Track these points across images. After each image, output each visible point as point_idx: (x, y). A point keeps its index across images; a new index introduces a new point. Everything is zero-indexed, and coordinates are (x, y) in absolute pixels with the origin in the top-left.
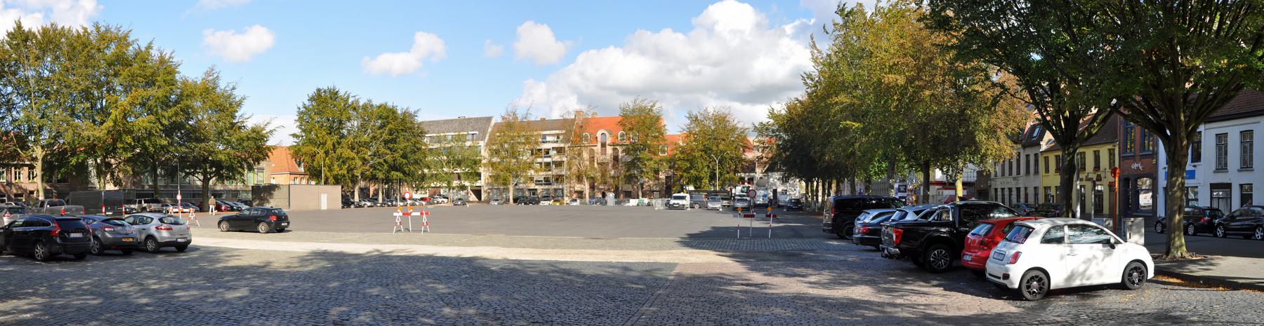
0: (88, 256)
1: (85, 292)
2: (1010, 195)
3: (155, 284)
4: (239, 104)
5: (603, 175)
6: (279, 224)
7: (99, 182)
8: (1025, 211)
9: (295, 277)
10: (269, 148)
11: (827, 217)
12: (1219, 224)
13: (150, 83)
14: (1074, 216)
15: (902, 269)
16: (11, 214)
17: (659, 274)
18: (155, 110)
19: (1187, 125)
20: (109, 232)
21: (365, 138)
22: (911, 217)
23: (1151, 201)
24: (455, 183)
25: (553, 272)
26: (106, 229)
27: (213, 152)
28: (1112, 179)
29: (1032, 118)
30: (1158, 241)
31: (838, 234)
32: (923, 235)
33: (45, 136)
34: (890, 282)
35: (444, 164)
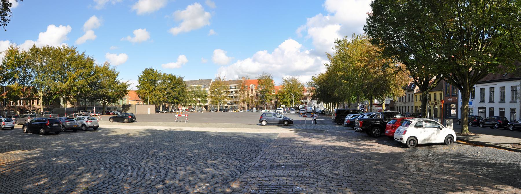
0: (60, 133)
1: (59, 146)
2: (403, 109)
3: (85, 142)
4: (117, 75)
5: (252, 101)
6: (132, 119)
7: (64, 105)
8: (408, 115)
9: (138, 139)
10: (128, 91)
11: (334, 117)
12: (481, 122)
13: (84, 67)
14: (427, 117)
15: (363, 136)
16: (31, 117)
17: (271, 138)
18: (85, 77)
19: (469, 85)
20: (68, 123)
21: (164, 87)
22: (366, 117)
23: (455, 113)
24: (198, 104)
25: (235, 136)
26: (67, 122)
27: (107, 93)
28: (441, 104)
29: (410, 81)
30: (458, 127)
31: (338, 123)
32: (370, 123)
33: (43, 89)
34: (358, 141)
35: (194, 97)
